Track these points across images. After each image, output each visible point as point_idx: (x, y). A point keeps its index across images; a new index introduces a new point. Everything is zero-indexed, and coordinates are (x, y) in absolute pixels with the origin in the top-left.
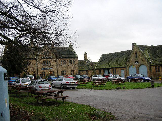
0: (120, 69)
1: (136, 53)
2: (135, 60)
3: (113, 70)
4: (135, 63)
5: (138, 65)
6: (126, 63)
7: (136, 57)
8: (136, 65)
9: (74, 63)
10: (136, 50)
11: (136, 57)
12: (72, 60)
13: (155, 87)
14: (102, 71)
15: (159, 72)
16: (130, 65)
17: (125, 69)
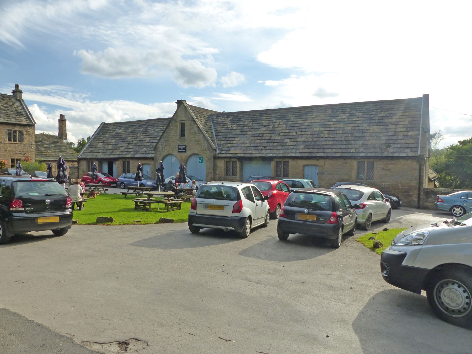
0: (301, 163)
1: (183, 125)
2: (179, 143)
3: (124, 163)
4: (185, 149)
5: (184, 155)
6: (155, 148)
7: (183, 134)
8: (181, 154)
9: (21, 140)
10: (182, 117)
11: (183, 134)
12: (15, 132)
13: (80, 224)
14: (96, 164)
15: (233, 175)
16: (164, 154)
17: (152, 162)
